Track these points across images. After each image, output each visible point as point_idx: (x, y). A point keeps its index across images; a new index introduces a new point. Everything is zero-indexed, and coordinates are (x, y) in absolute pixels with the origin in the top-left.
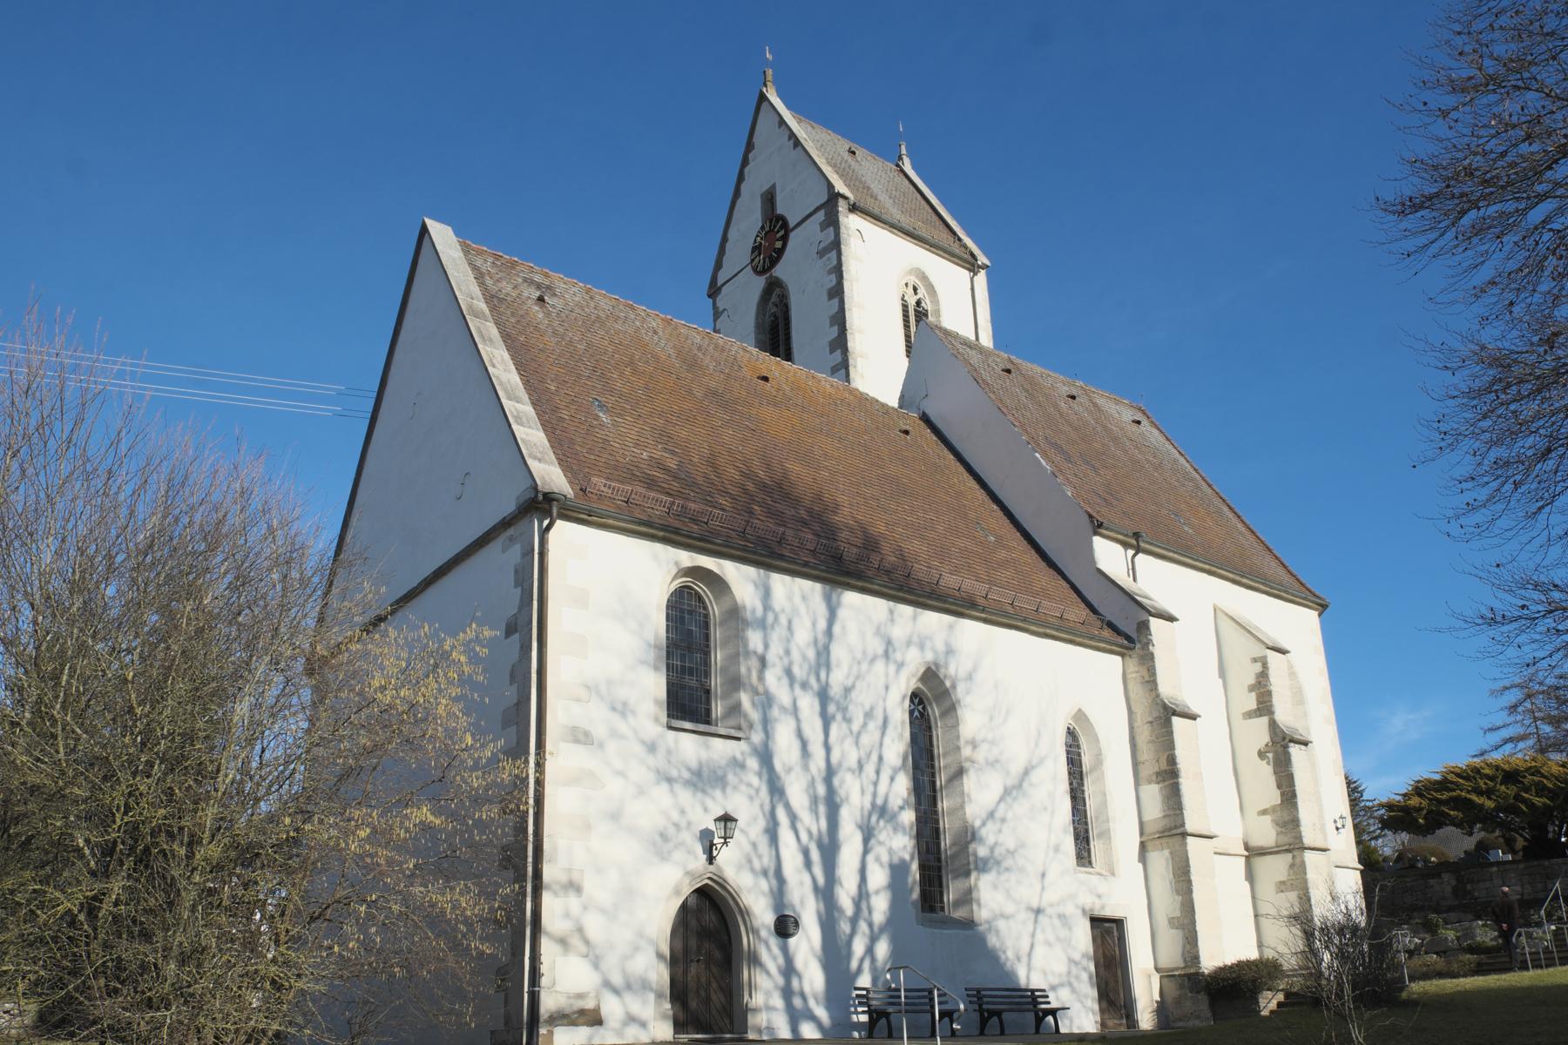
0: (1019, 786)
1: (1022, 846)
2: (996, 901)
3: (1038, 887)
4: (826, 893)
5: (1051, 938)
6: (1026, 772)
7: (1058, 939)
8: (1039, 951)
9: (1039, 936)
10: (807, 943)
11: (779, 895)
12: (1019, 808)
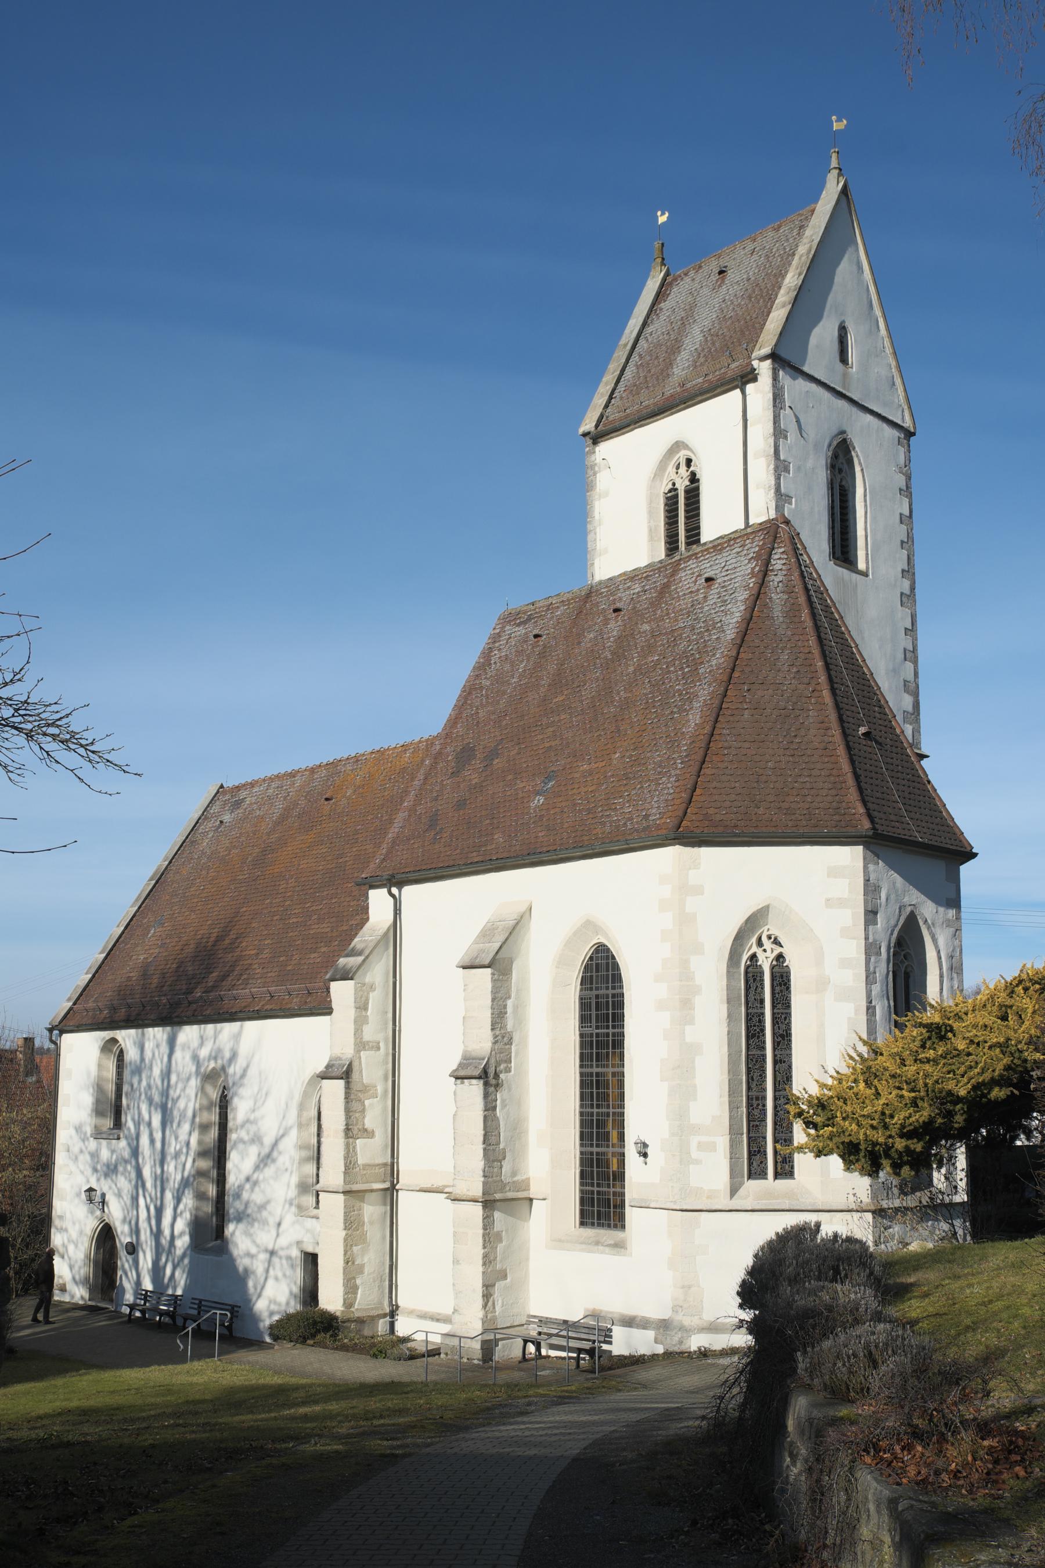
0: (268, 1156)
1: (268, 1202)
2: (242, 1241)
3: (274, 1233)
4: (157, 1234)
5: (280, 1275)
6: (275, 1144)
7: (284, 1275)
8: (270, 1282)
9: (271, 1272)
10: (146, 1260)
11: (136, 1231)
12: (269, 1171)
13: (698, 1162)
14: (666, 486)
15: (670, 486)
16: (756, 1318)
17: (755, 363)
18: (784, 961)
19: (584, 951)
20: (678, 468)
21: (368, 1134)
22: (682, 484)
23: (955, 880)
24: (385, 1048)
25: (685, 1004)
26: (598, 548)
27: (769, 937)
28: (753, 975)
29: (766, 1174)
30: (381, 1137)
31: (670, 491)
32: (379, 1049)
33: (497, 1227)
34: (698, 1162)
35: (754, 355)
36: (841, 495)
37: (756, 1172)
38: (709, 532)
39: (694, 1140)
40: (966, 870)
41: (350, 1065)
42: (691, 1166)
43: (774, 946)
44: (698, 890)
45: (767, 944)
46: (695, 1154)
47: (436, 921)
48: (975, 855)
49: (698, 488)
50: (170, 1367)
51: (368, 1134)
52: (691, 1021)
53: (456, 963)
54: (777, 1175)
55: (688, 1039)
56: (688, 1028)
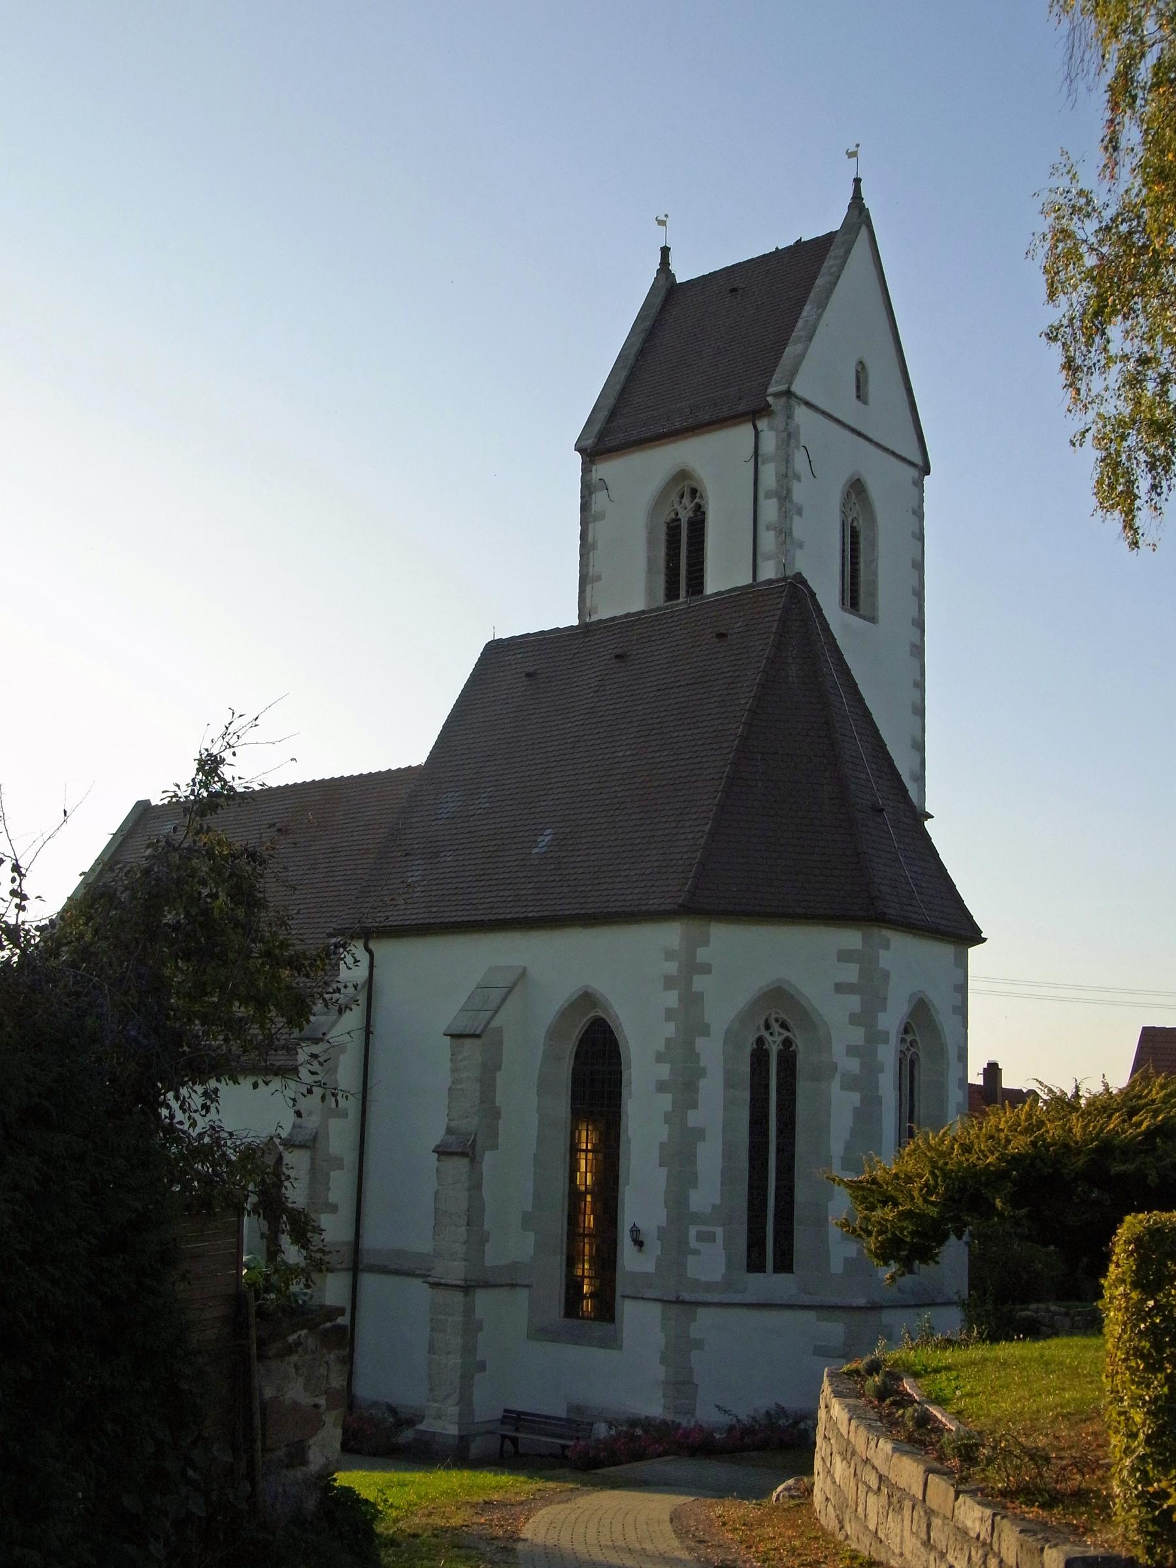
13: (697, 1252)
14: (667, 516)
15: (673, 515)
17: (770, 399)
19: (583, 1023)
20: (682, 497)
21: (333, 1208)
22: (685, 516)
23: (962, 963)
25: (685, 1087)
26: (591, 574)
27: (777, 1021)
28: (759, 1057)
29: (765, 1267)
30: (346, 1211)
31: (673, 520)
33: (479, 1313)
34: (697, 1252)
35: (771, 390)
36: (852, 536)
37: (755, 1264)
39: (693, 1231)
40: (974, 952)
41: (317, 1133)
43: (782, 1031)
44: (706, 969)
45: (776, 1027)
46: (693, 1244)
47: (425, 985)
48: (984, 940)
49: (703, 522)
50: (466, 1473)
52: (694, 1105)
53: (443, 1029)
54: (777, 1270)
55: (691, 1124)
56: (690, 1112)
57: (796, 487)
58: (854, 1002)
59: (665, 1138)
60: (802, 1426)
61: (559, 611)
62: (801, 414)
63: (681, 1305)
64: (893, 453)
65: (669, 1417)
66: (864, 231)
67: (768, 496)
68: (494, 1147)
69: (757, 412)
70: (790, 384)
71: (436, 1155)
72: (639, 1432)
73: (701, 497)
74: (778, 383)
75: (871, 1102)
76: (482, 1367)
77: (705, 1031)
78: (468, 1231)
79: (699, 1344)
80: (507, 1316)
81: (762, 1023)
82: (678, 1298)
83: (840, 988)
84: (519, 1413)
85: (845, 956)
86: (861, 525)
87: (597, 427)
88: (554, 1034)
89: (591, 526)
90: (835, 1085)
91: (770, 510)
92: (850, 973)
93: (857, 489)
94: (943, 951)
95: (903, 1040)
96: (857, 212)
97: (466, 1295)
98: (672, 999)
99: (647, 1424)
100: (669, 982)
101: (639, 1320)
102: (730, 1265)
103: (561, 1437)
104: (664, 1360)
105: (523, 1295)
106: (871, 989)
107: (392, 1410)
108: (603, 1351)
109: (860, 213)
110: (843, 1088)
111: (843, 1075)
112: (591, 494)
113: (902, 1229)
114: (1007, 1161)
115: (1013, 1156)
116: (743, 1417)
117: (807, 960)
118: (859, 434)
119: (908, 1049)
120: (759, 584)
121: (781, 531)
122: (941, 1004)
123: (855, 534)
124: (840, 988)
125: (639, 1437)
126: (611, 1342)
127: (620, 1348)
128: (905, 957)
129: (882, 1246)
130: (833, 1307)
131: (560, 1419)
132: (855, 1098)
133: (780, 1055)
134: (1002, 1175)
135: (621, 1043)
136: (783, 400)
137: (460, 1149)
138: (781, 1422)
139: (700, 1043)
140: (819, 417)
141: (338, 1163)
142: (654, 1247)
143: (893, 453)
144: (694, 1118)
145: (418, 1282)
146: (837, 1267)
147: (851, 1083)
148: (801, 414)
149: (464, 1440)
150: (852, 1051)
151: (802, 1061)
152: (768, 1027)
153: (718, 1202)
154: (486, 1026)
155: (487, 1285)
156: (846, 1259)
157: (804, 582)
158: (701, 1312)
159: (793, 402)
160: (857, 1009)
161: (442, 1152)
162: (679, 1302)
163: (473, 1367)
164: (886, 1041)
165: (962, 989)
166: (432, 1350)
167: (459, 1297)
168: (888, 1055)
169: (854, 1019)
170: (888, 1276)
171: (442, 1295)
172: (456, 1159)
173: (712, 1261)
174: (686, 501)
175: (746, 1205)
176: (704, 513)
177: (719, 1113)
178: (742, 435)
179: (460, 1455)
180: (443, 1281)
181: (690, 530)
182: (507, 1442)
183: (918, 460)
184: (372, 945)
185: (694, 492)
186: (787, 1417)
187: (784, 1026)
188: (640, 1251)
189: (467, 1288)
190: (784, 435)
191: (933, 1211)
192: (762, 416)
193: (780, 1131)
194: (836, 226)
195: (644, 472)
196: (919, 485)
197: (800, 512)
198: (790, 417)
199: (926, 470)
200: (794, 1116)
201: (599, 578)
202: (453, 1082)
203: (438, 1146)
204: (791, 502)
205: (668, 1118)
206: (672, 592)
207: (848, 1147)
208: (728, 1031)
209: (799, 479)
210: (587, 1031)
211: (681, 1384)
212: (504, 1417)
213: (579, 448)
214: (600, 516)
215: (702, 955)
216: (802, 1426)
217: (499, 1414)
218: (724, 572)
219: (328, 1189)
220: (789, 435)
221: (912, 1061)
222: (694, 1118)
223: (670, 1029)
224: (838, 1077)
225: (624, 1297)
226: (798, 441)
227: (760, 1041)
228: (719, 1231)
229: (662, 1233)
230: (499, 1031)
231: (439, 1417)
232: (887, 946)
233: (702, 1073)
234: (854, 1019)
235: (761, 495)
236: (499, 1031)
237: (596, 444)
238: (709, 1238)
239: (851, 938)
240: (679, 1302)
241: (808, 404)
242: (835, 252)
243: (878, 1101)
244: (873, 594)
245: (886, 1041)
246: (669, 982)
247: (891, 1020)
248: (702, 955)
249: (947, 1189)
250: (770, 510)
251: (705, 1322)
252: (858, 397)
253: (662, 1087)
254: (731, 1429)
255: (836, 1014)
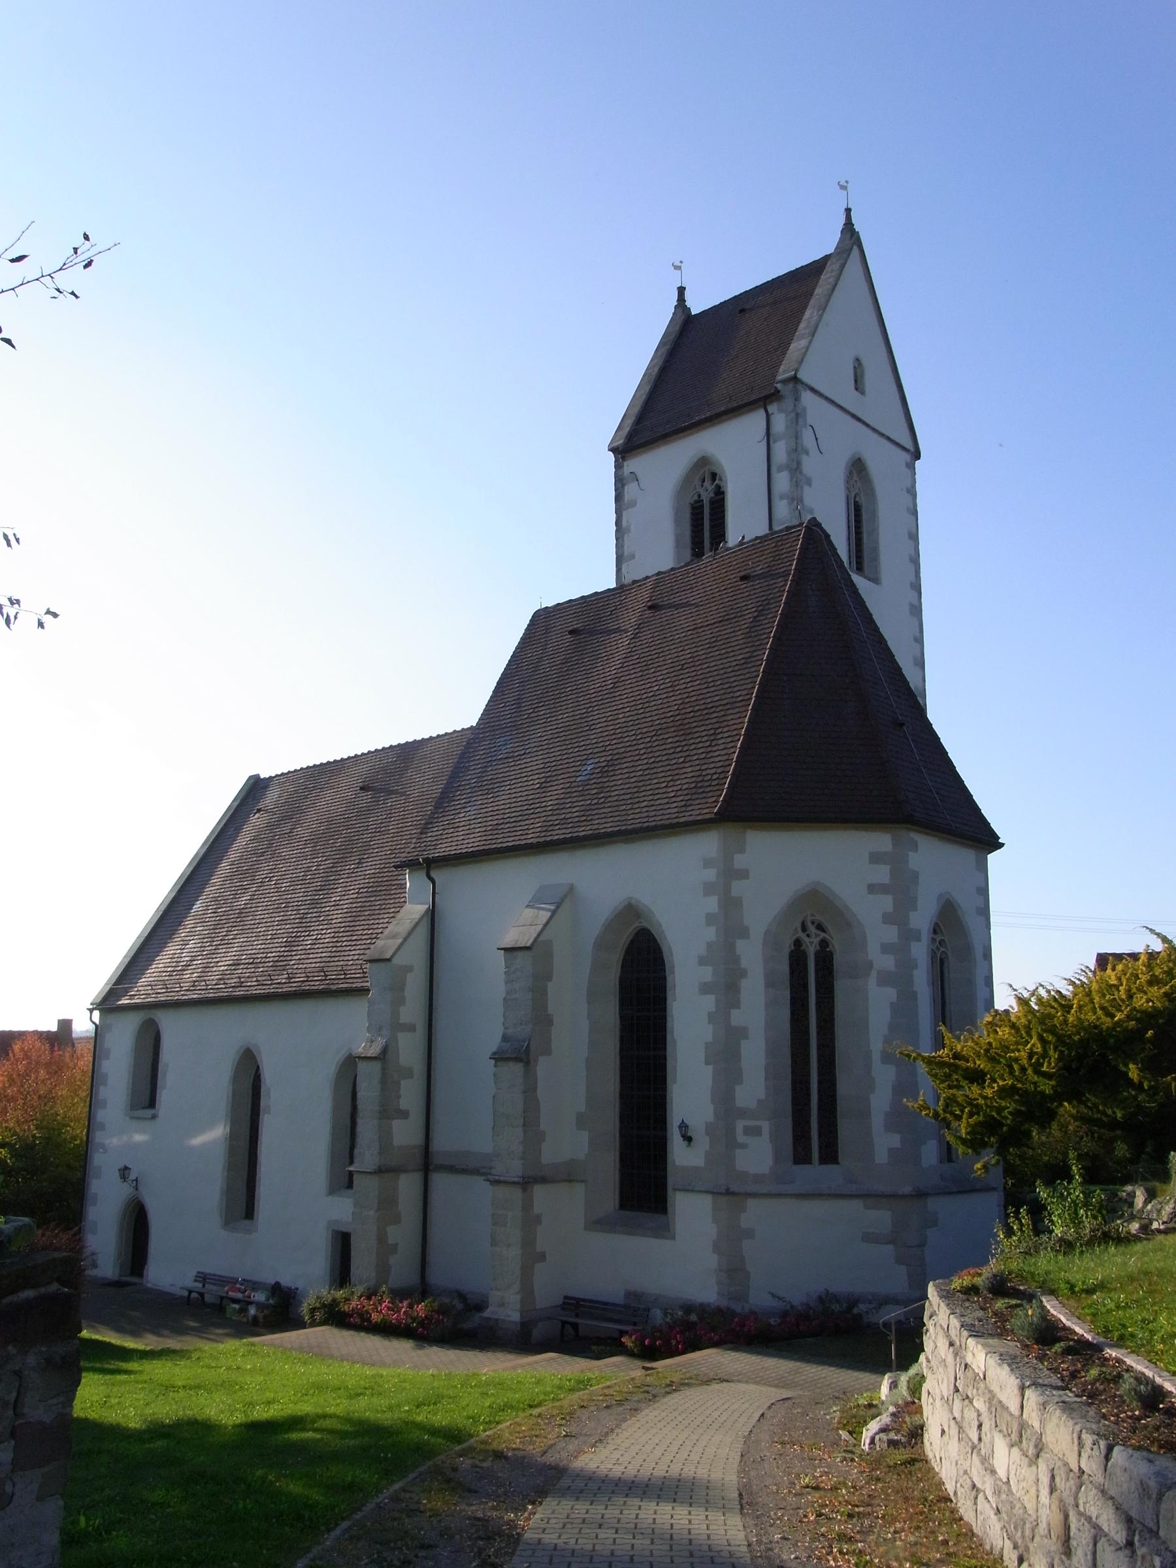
13: (743, 1146)
14: (690, 498)
15: (696, 498)
16: (67, 1375)
17: (779, 386)
18: (828, 946)
20: (703, 481)
21: (404, 1115)
22: (706, 497)
23: (983, 868)
24: (421, 1030)
25: (728, 987)
27: (813, 923)
28: (797, 958)
29: (811, 1158)
31: (696, 502)
32: (415, 1030)
33: (537, 1209)
34: (743, 1146)
35: (779, 378)
37: (801, 1157)
38: (733, 538)
39: (740, 1125)
42: (737, 1151)
43: (818, 932)
44: (743, 874)
45: (812, 929)
46: (741, 1138)
48: (1002, 845)
49: (723, 500)
51: (404, 1115)
52: (737, 1005)
57: (805, 461)
58: (886, 902)
59: (710, 1039)
60: (855, 1311)
61: (600, 576)
62: (807, 397)
63: (730, 1194)
64: (888, 439)
65: (724, 1303)
66: (855, 250)
67: (780, 470)
68: (548, 1052)
69: (767, 399)
70: (797, 370)
71: (493, 1061)
72: (694, 1318)
73: (721, 479)
74: (785, 372)
75: (907, 996)
76: (542, 1257)
77: (744, 933)
78: (524, 1131)
79: (750, 1234)
80: (564, 1210)
81: (799, 925)
82: (728, 1189)
83: (872, 888)
84: (578, 1300)
85: (875, 858)
86: (862, 500)
87: (627, 430)
88: (601, 944)
89: (624, 513)
90: (872, 981)
91: (782, 482)
92: (882, 874)
93: (858, 468)
94: (966, 855)
95: (933, 940)
96: (848, 236)
97: (525, 1190)
98: (712, 904)
99: (702, 1310)
100: (709, 889)
101: (692, 1213)
102: (777, 1160)
103: (618, 1321)
104: (717, 1248)
105: (579, 1190)
106: (902, 888)
107: (462, 1296)
108: (657, 1241)
109: (852, 236)
110: (879, 985)
111: (879, 972)
112: (623, 486)
113: (1000, 1110)
114: (1137, 1020)
115: (1144, 1012)
116: (796, 1303)
117: (839, 862)
118: (859, 420)
119: (938, 949)
120: (776, 532)
121: (793, 500)
122: (966, 904)
123: (858, 509)
124: (872, 888)
125: (694, 1324)
126: (665, 1231)
127: (674, 1238)
128: (932, 858)
129: (973, 1131)
130: (876, 1196)
131: (617, 1305)
132: (891, 993)
133: (817, 954)
134: (1136, 1036)
135: (667, 965)
136: (791, 385)
137: (517, 1054)
138: (833, 1307)
139: (741, 945)
140: (824, 402)
141: (409, 1073)
142: (703, 1142)
143: (888, 439)
144: (737, 1017)
145: (479, 1182)
146: (881, 1156)
147: (885, 979)
148: (807, 397)
149: (526, 1326)
150: (886, 948)
151: (838, 960)
152: (804, 928)
153: (763, 1097)
154: (536, 939)
155: (543, 1180)
156: (890, 1150)
157: (819, 525)
158: (752, 1203)
159: (800, 387)
160: (890, 909)
161: (499, 1057)
162: (728, 1193)
163: (532, 1257)
164: (919, 940)
165: (984, 891)
166: (494, 1243)
167: (517, 1194)
168: (920, 951)
169: (887, 919)
170: (979, 1166)
171: (503, 1192)
172: (511, 1064)
173: (758, 1155)
174: (707, 483)
175: (789, 1099)
176: (723, 493)
177: (759, 1010)
178: (754, 422)
179: (524, 1340)
180: (502, 1179)
181: (712, 509)
182: (568, 1327)
183: (909, 444)
184: (433, 874)
185: (714, 476)
186: (838, 1301)
187: (820, 927)
188: (689, 1145)
189: (526, 1183)
190: (793, 415)
191: (1047, 1086)
192: (771, 402)
193: (820, 1028)
194: (830, 249)
195: (668, 464)
196: (912, 467)
197: (809, 482)
198: (797, 399)
199: (917, 455)
200: (833, 1013)
201: (632, 557)
202: (508, 993)
203: (495, 1053)
204: (801, 473)
205: (711, 1018)
206: (697, 551)
207: (887, 1041)
208: (767, 933)
209: (807, 453)
210: (632, 942)
211: (734, 1271)
212: (564, 1303)
213: (613, 450)
214: (633, 504)
215: (740, 861)
216: (855, 1311)
217: (560, 1301)
218: (744, 522)
219: (399, 1097)
220: (797, 415)
221: (941, 960)
222: (737, 1017)
223: (711, 934)
224: (874, 973)
225: (675, 1190)
226: (805, 421)
227: (798, 943)
228: (766, 1126)
229: (710, 1129)
230: (549, 943)
231: (502, 1305)
232: (915, 848)
233: (743, 974)
234: (887, 919)
235: (774, 469)
236: (549, 943)
237: (625, 444)
238: (755, 1131)
239: (881, 840)
240: (728, 1193)
241: (813, 390)
242: (826, 278)
243: (913, 996)
244: (875, 559)
245: (919, 940)
246: (709, 889)
247: (922, 918)
248: (740, 861)
249: (1059, 1059)
250: (782, 482)
251: (755, 1213)
252: (857, 389)
253: (705, 989)
254: (784, 1314)
255: (869, 912)
